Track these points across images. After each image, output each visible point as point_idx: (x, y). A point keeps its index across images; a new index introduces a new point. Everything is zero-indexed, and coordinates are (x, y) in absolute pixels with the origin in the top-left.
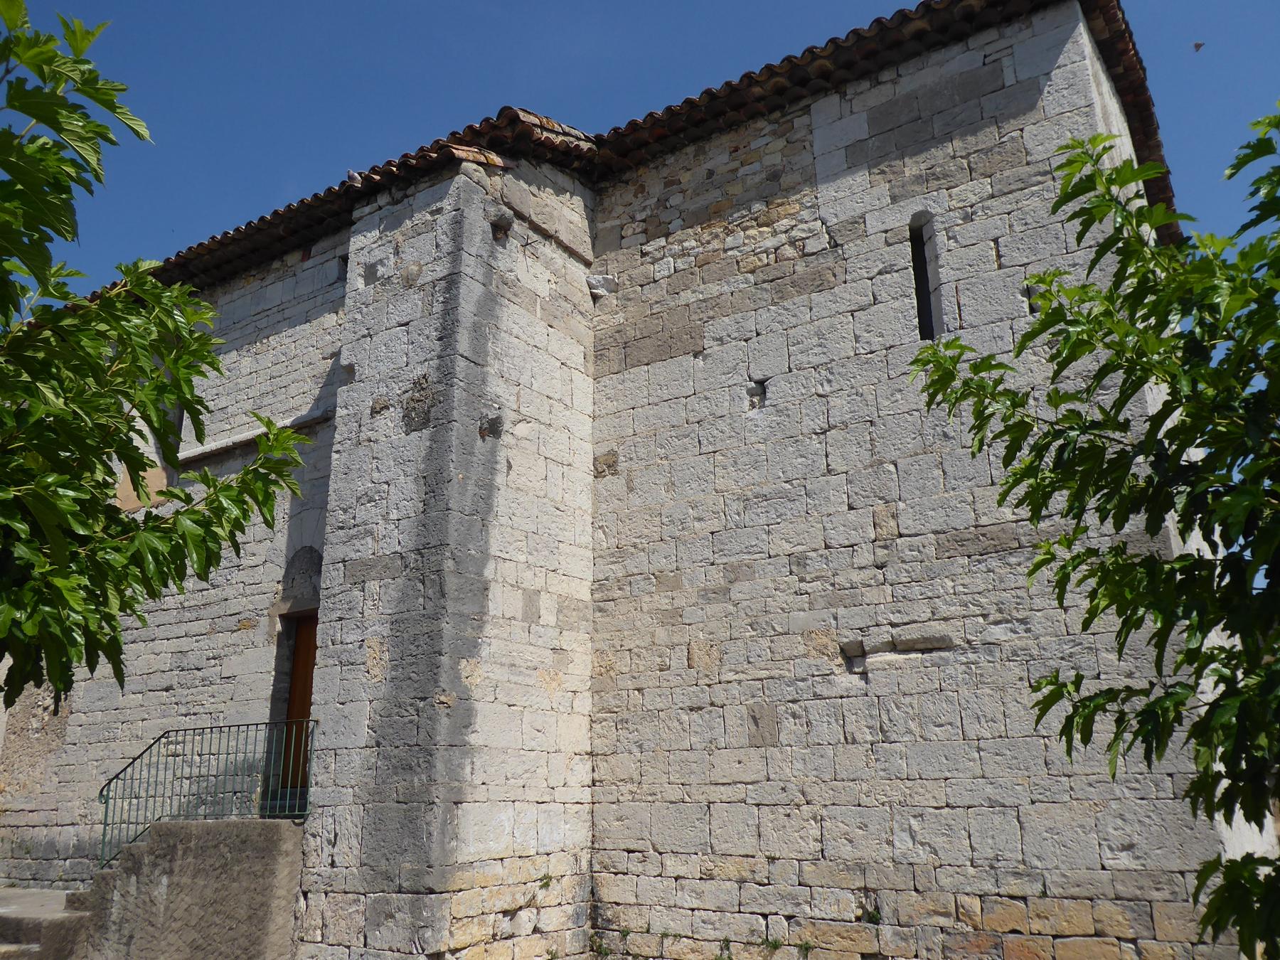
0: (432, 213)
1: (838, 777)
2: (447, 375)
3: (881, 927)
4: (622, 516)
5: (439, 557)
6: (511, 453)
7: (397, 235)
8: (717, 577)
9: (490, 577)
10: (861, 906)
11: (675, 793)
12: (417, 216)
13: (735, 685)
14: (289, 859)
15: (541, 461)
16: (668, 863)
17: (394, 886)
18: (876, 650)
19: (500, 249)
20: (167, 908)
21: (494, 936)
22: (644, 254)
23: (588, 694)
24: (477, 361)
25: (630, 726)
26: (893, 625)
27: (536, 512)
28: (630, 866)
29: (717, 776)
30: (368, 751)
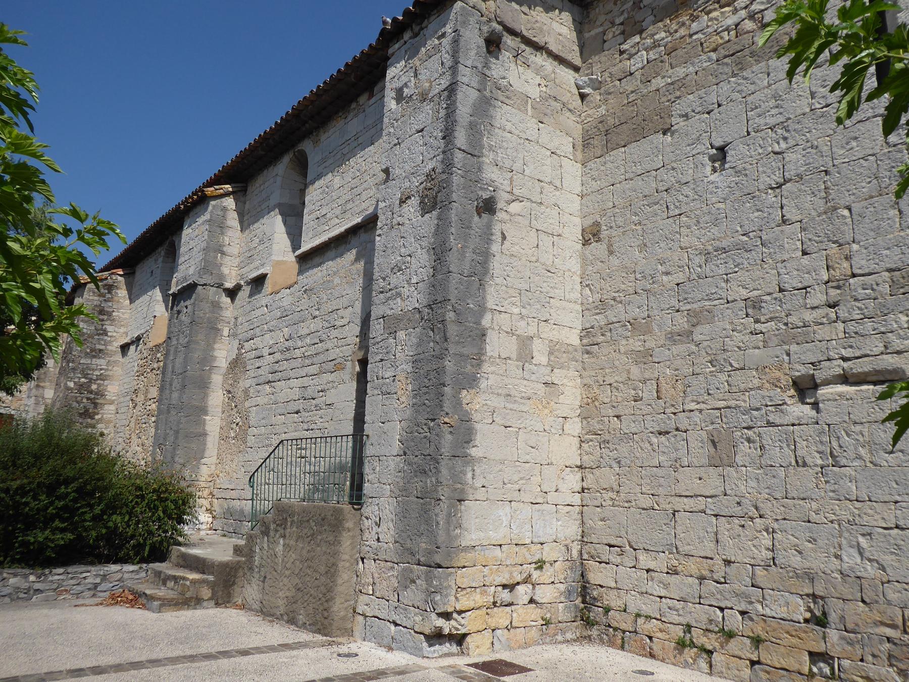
0: (439, 38)
1: (789, 495)
2: (448, 165)
3: (828, 630)
4: (604, 275)
5: (443, 310)
6: (506, 227)
7: (416, 61)
8: (682, 322)
9: (488, 326)
10: (809, 610)
11: (647, 502)
12: (429, 42)
13: (697, 413)
14: (351, 534)
15: (533, 233)
16: (641, 558)
17: (415, 560)
18: (827, 383)
19: (493, 60)
20: (283, 561)
21: (494, 603)
22: (622, 53)
23: (578, 420)
24: (475, 153)
25: (610, 445)
26: (844, 359)
27: (528, 274)
28: (611, 557)
29: (681, 489)
30: (399, 458)
